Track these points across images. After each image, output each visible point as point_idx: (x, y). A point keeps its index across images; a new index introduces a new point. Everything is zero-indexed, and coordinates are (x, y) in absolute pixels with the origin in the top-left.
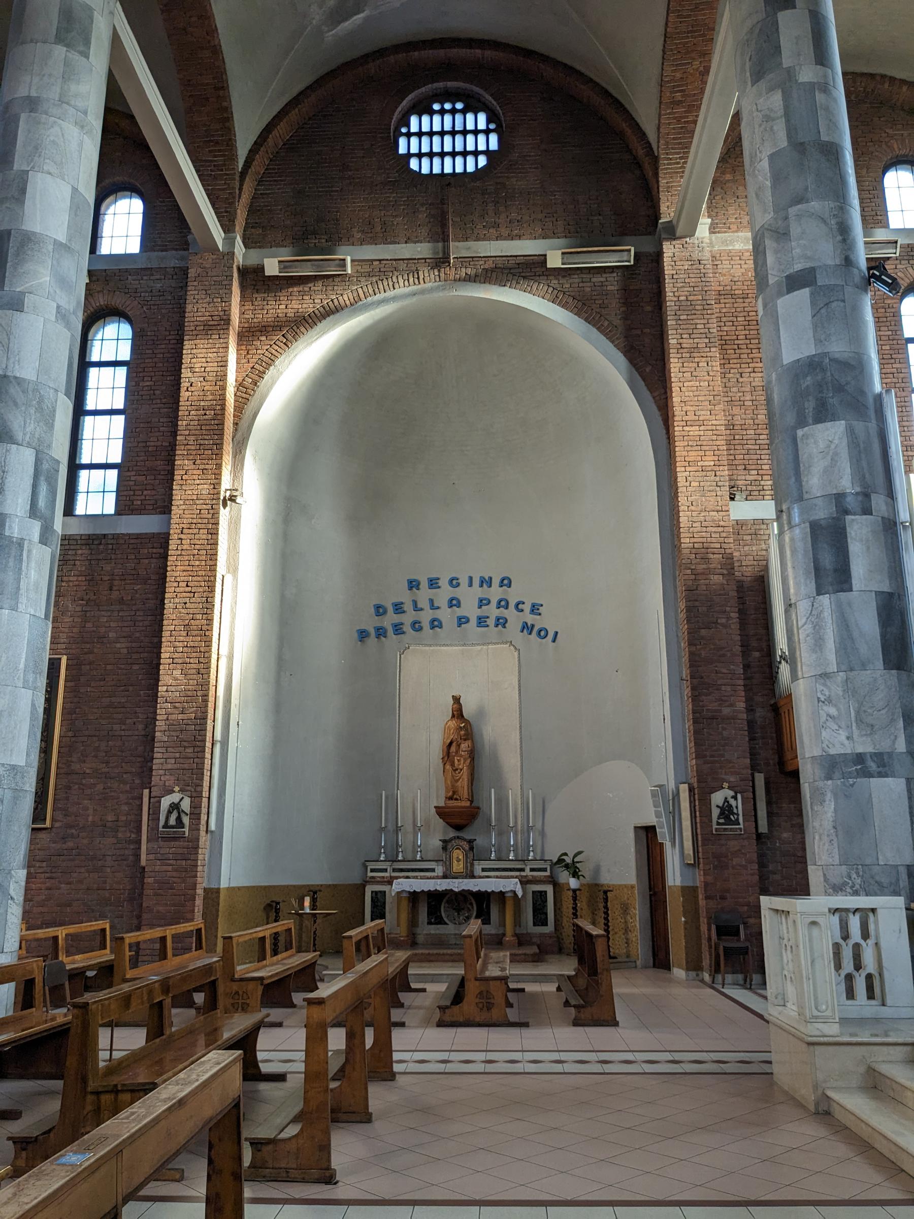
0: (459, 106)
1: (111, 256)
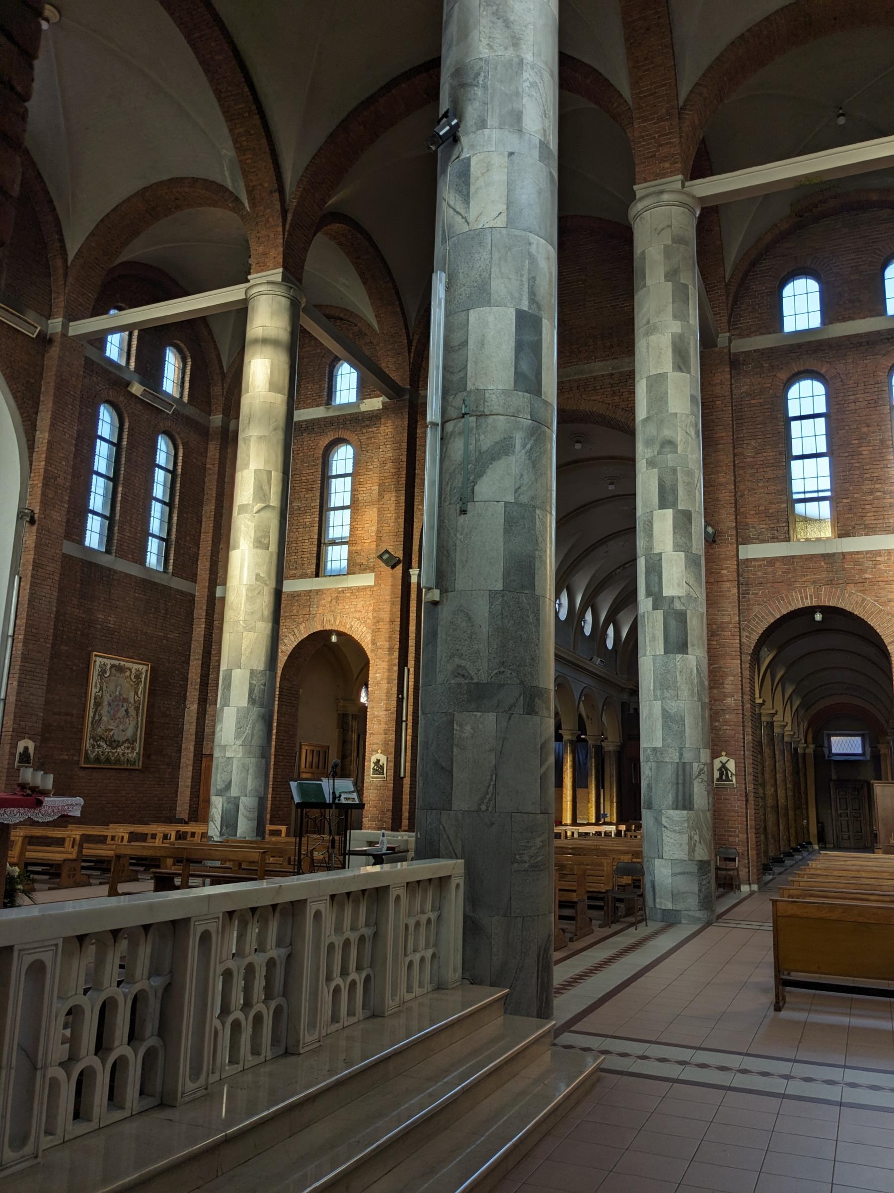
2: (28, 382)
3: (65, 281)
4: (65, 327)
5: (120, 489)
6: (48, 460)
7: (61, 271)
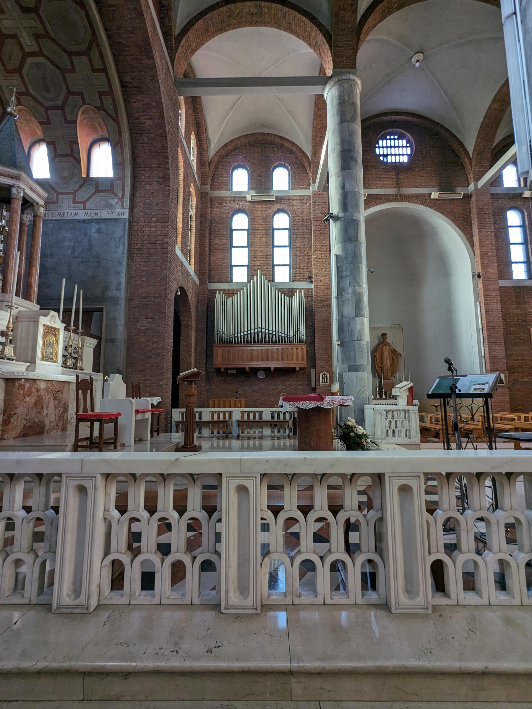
0: (396, 137)
2: (464, 218)
3: (471, 166)
4: (476, 185)
5: (529, 246)
6: (481, 248)
7: (468, 163)
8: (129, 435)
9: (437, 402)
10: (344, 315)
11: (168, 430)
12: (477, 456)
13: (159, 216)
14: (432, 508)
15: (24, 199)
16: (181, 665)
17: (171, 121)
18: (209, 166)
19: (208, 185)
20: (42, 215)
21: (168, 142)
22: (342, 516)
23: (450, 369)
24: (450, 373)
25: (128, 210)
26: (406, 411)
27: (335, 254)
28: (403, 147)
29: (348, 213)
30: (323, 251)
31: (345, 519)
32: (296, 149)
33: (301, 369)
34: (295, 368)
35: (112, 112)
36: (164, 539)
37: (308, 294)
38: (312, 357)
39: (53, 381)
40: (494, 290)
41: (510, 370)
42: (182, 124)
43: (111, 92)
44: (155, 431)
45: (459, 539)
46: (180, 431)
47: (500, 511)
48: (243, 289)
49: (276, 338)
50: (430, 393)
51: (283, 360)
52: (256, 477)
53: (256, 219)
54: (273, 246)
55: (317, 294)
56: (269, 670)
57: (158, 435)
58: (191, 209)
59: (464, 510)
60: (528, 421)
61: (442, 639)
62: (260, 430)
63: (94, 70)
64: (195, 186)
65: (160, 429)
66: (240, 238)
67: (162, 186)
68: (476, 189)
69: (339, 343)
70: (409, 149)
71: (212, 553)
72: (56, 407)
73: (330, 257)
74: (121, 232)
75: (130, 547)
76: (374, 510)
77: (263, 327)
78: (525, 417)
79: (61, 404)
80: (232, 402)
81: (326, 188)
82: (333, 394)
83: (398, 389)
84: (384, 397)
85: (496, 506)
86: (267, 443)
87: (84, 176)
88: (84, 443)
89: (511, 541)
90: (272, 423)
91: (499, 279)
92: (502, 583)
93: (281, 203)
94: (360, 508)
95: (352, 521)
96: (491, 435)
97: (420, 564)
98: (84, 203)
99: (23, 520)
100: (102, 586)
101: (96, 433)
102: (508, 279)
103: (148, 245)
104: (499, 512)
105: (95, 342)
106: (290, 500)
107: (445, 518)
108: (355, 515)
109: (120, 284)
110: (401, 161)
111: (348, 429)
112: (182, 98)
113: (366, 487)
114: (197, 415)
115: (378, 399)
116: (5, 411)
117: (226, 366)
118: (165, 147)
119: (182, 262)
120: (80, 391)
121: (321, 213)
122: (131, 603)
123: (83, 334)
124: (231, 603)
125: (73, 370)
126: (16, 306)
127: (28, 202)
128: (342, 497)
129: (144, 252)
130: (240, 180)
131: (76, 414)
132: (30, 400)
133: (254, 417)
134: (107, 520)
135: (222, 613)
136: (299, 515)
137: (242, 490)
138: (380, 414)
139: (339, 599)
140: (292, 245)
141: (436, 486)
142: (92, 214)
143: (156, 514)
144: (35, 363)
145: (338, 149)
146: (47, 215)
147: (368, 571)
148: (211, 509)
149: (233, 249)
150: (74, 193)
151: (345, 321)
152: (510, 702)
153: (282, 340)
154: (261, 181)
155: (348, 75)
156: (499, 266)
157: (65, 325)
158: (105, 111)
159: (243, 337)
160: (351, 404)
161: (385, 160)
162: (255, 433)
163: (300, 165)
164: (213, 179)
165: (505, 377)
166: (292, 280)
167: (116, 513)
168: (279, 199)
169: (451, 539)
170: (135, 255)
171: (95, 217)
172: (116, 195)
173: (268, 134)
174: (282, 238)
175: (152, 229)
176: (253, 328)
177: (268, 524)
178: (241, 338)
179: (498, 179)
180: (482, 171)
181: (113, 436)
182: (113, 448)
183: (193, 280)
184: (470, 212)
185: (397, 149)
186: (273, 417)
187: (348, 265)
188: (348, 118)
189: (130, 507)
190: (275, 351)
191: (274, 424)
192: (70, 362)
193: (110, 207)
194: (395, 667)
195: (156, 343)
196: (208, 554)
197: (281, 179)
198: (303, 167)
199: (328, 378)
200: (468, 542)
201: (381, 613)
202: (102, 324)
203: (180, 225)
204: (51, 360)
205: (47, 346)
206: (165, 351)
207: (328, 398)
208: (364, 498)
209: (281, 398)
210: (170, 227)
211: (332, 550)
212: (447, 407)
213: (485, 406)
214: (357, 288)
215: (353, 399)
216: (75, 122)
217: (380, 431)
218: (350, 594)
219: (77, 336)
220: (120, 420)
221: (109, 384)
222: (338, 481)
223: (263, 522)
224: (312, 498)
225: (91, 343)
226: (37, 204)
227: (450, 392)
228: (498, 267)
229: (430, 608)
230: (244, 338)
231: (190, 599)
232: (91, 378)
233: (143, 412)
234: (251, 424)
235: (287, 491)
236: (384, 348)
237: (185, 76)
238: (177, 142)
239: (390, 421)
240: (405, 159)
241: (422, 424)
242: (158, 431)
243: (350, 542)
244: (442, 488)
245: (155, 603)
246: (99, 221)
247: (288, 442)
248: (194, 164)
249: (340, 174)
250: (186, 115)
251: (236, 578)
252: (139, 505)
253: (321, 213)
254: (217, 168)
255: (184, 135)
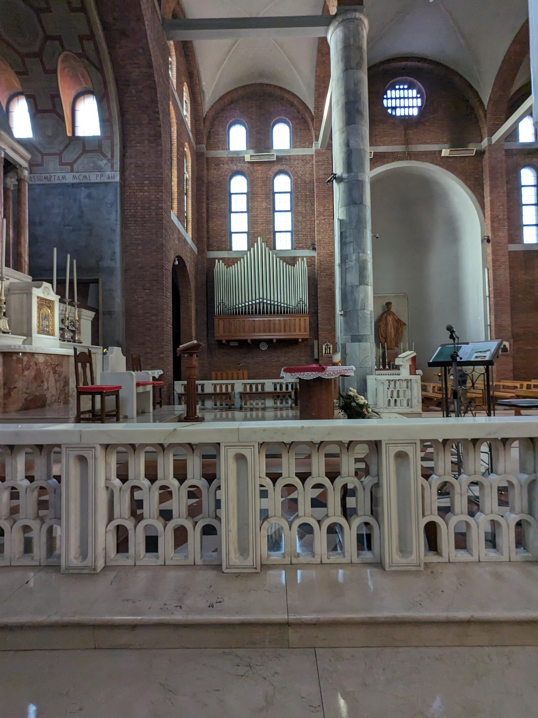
0: (406, 87)
1: (524, 144)
3: (486, 119)
4: (490, 141)
6: (491, 210)
7: (482, 115)
8: (131, 407)
9: (438, 371)
10: (347, 283)
11: (171, 402)
12: (475, 422)
13: (152, 179)
14: (428, 473)
15: (5, 160)
16: (185, 618)
17: (161, 71)
18: (204, 123)
19: (203, 144)
20: (26, 179)
21: (158, 95)
22: (339, 482)
23: (452, 337)
24: (451, 341)
25: (118, 173)
26: (407, 381)
27: (338, 219)
28: (413, 98)
29: (353, 174)
30: (326, 216)
31: (342, 485)
32: (298, 102)
33: (304, 340)
34: (298, 339)
35: (96, 61)
36: (166, 506)
37: (311, 262)
38: (314, 328)
39: (51, 354)
40: (503, 255)
41: (515, 338)
42: (173, 74)
43: (92, 37)
44: (158, 403)
45: (452, 502)
46: (183, 403)
47: (494, 475)
48: (244, 258)
49: (278, 308)
50: (431, 361)
51: (285, 331)
52: (254, 446)
53: (255, 182)
54: (274, 211)
55: (320, 262)
56: (267, 622)
57: (161, 407)
58: (187, 171)
59: (460, 474)
60: (530, 389)
61: (432, 592)
62: (263, 401)
63: (74, 10)
64: (189, 145)
65: (162, 401)
66: (239, 203)
67: (153, 145)
68: (490, 145)
69: (342, 313)
70: (419, 100)
71: (213, 518)
72: (56, 381)
73: (333, 223)
74: (112, 197)
75: (133, 513)
76: (371, 476)
77: (265, 297)
78: (527, 385)
79: (62, 377)
80: (235, 375)
81: (329, 146)
82: (334, 364)
83: (401, 359)
84: (387, 367)
85: (491, 470)
86: (269, 414)
87: (69, 134)
88: (87, 416)
89: (503, 503)
90: (275, 394)
91: (509, 243)
92: (492, 541)
93: (282, 163)
94: (356, 474)
95: (350, 486)
96: (490, 404)
97: (414, 525)
98: (71, 164)
99: (26, 489)
100: (108, 549)
101: (98, 406)
102: (519, 243)
103: (142, 211)
104: (493, 476)
105: (92, 314)
106: (289, 468)
107: (439, 482)
108: (352, 482)
109: (114, 253)
110: (411, 114)
111: (350, 399)
112: (172, 42)
113: (365, 454)
114: (200, 388)
115: (381, 370)
116: (5, 384)
117: (227, 338)
118: (154, 101)
119: (178, 230)
120: (80, 365)
121: (325, 174)
122: (137, 564)
123: (79, 307)
124: (232, 563)
125: (71, 343)
126: (7, 277)
127: (11, 164)
128: (339, 465)
129: (138, 219)
130: (238, 138)
131: (77, 387)
132: (30, 374)
133: (257, 389)
134: (109, 489)
135: (223, 572)
136: (297, 482)
137: (240, 458)
138: (382, 384)
139: (335, 558)
140: (294, 209)
141: (432, 453)
142: (81, 177)
143: (157, 482)
144: (31, 336)
145: (342, 101)
146: (33, 179)
147: (364, 533)
148: (210, 477)
149: (232, 215)
150: (60, 154)
151: (349, 289)
152: (492, 646)
153: (284, 311)
154: (260, 139)
155: (354, 14)
156: (509, 230)
157: (59, 297)
158: (88, 59)
159: (244, 308)
160: (352, 374)
161: (394, 113)
162: (257, 404)
163: (302, 121)
164: (209, 137)
165: (510, 345)
166: (294, 248)
167: (117, 482)
168: (280, 159)
169: (445, 502)
170: (129, 222)
171: (85, 181)
172: (105, 156)
173: (267, 84)
174: (283, 202)
175: (145, 194)
176: (254, 298)
177: (267, 491)
178: (242, 309)
179: (513, 133)
180: (497, 125)
181: (115, 408)
182: (115, 420)
183: (191, 248)
184: (482, 171)
185: (406, 100)
186: (275, 389)
187: (352, 229)
188: (353, 64)
189: (131, 475)
190: (277, 322)
191: (276, 396)
192: (68, 335)
193: (99, 169)
194: (385, 618)
195: (154, 315)
196: (209, 519)
197: (281, 136)
198: (305, 122)
199: (331, 349)
200: (461, 504)
201: (375, 570)
202: (98, 295)
203: (175, 189)
204: (48, 333)
205: (42, 319)
206: (165, 324)
207: (330, 368)
208: (362, 466)
209: (283, 369)
210: (164, 191)
211: (330, 515)
212: (448, 375)
213: (485, 374)
214: (361, 254)
215: (354, 368)
216: (55, 72)
217: (382, 401)
218: (346, 554)
219: (73, 308)
220: (122, 393)
221: (108, 356)
222: (334, 449)
223: (262, 488)
224: (310, 465)
225: (88, 315)
226: (21, 166)
227: (451, 360)
228: (508, 230)
229: (422, 565)
230: (245, 309)
231: (478, 556)
232: (89, 351)
233: (144, 384)
234: (253, 395)
235: (285, 459)
236: (389, 317)
237: (175, 16)
238: (168, 95)
239: (392, 391)
240: (415, 112)
241: (425, 393)
242: (160, 404)
243: (347, 507)
244: (438, 454)
245: (160, 564)
246: (89, 185)
247: (291, 413)
248: (188, 121)
249: (344, 129)
250: (177, 63)
251: (236, 541)
252: (139, 474)
253: (325, 174)
254: (212, 125)
255: (175, 87)
